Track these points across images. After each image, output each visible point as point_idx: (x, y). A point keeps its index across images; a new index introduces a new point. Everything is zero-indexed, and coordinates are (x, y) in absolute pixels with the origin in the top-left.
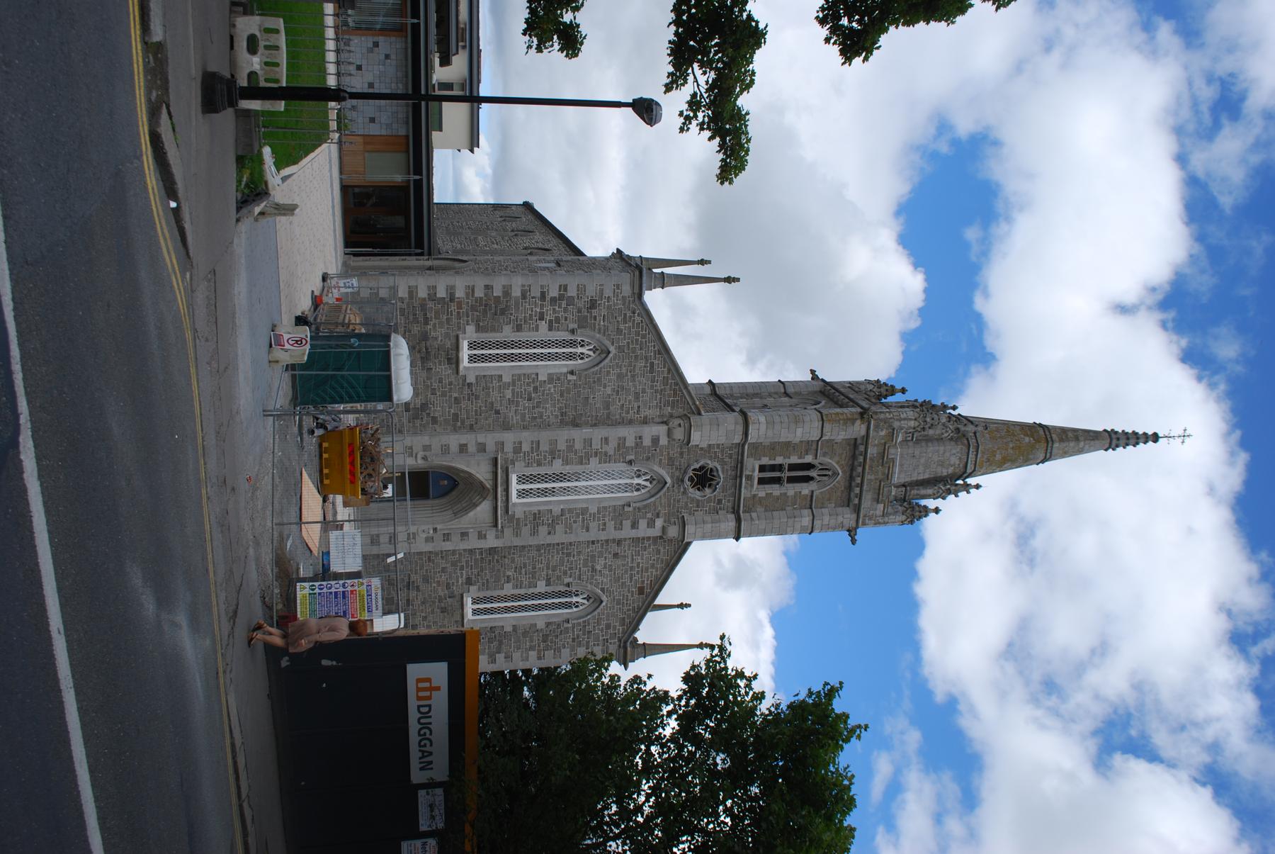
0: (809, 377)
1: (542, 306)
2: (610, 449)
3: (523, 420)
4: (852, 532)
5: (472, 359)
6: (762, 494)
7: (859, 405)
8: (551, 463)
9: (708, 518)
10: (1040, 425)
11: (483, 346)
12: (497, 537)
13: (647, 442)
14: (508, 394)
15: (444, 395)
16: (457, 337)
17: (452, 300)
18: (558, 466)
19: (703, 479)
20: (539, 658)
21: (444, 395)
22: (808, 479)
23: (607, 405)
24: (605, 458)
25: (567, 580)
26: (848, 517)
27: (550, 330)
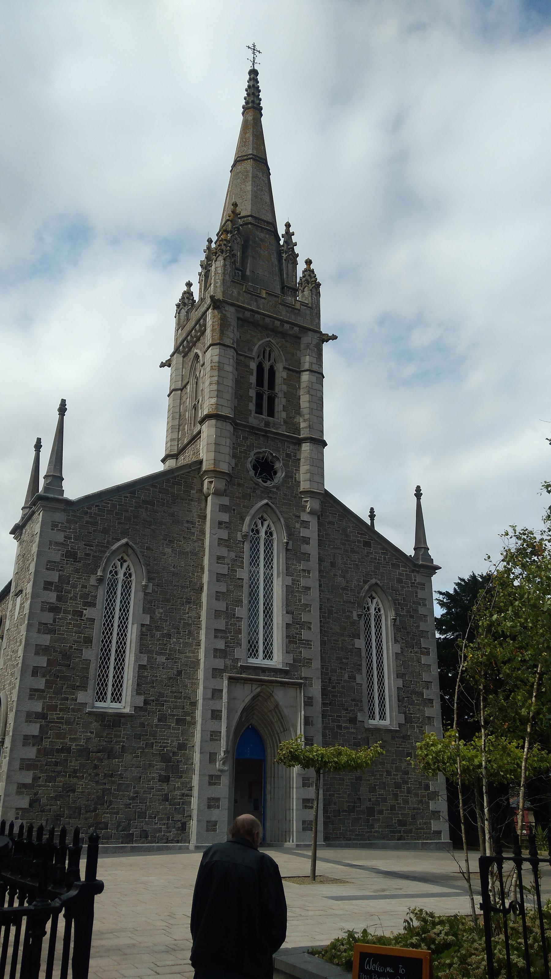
0: (167, 369)
1: (66, 612)
7: (205, 313)
10: (234, 166)
11: (103, 684)
14: (162, 659)
18: (242, 612)
19: (265, 468)
20: (428, 653)
22: (272, 372)
26: (308, 339)
27: (94, 605)
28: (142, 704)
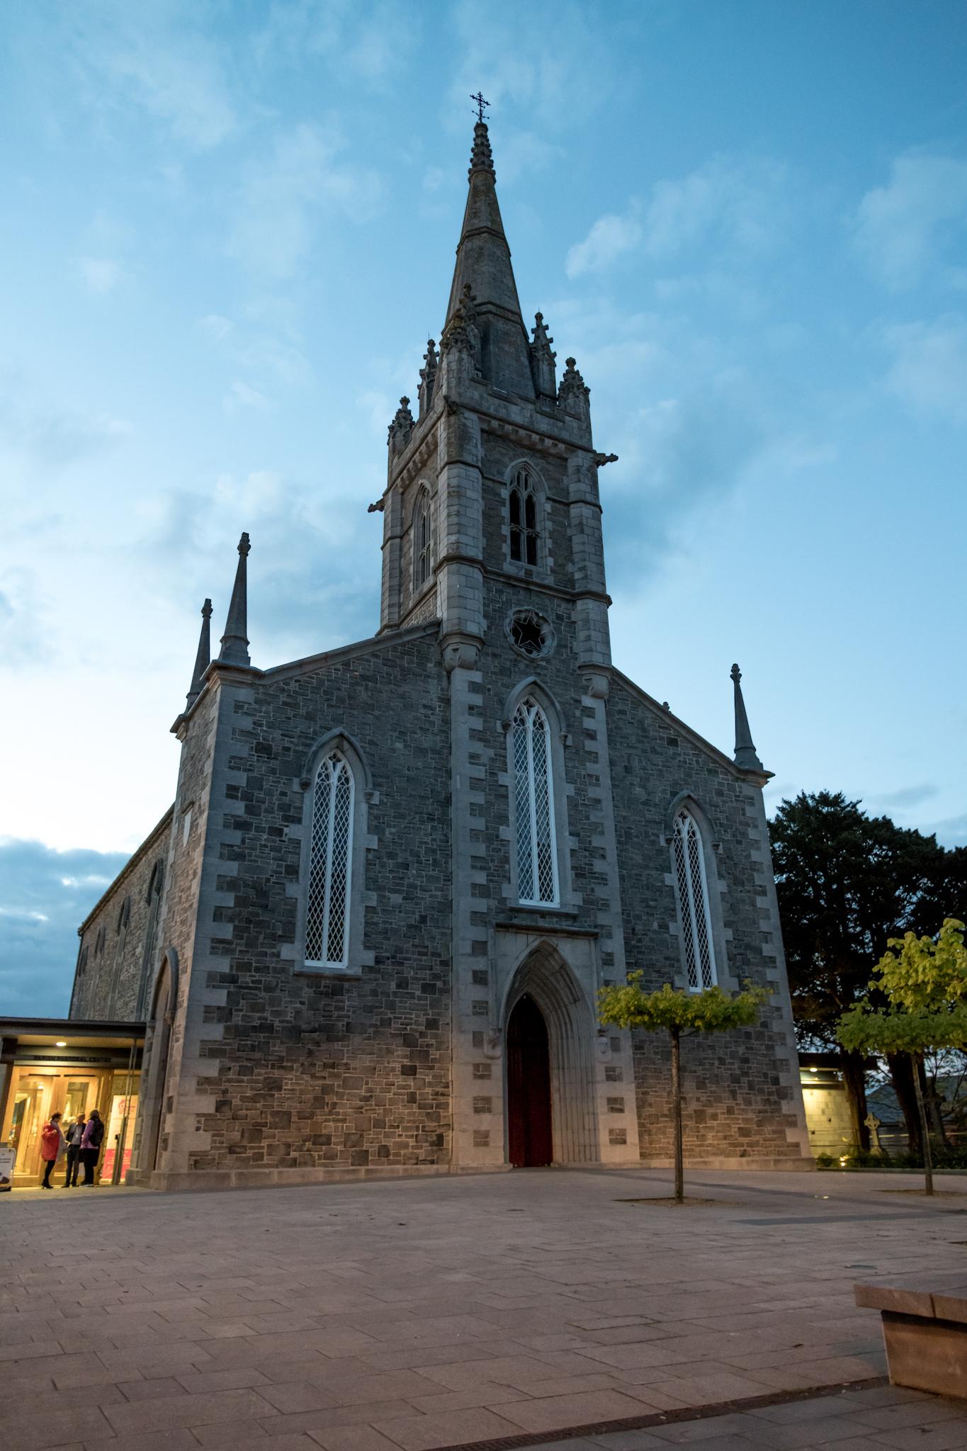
0: (379, 515)
1: (259, 829)
2: (487, 753)
3: (437, 879)
4: (603, 460)
5: (335, 954)
6: (550, 561)
8: (505, 843)
9: (582, 635)
11: (315, 934)
12: (610, 936)
13: (478, 700)
14: (396, 899)
15: (392, 1007)
16: (298, 975)
17: (232, 979)
19: (528, 633)
21: (392, 1007)
22: (530, 504)
23: (421, 751)
24: (499, 763)
25: (663, 843)
27: (299, 821)
28: (372, 963)
